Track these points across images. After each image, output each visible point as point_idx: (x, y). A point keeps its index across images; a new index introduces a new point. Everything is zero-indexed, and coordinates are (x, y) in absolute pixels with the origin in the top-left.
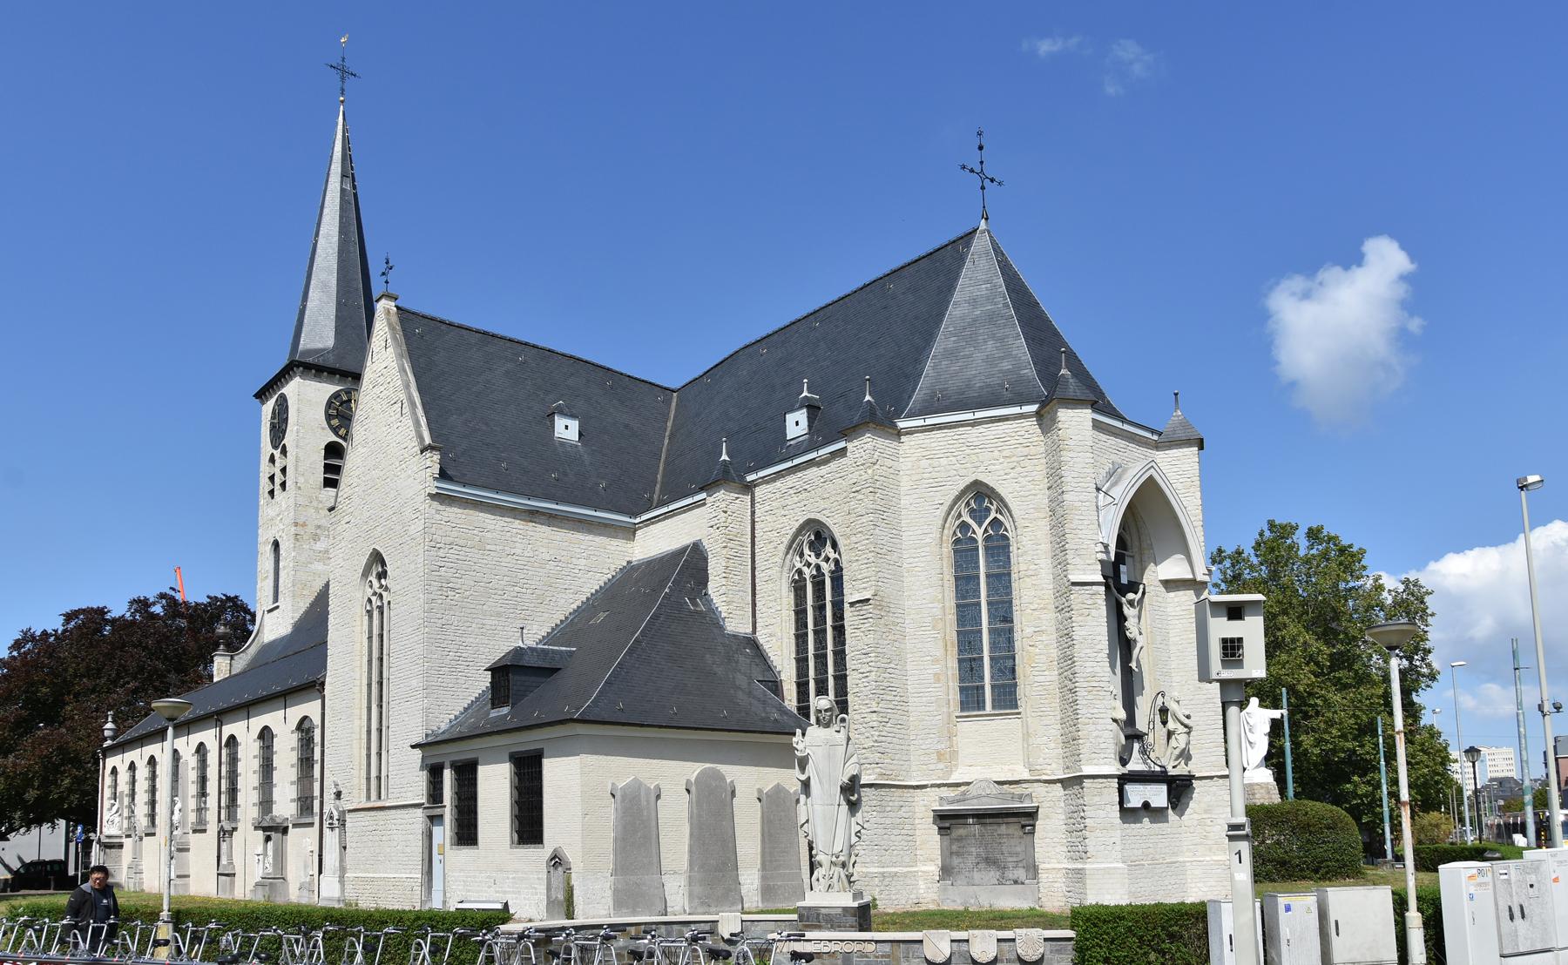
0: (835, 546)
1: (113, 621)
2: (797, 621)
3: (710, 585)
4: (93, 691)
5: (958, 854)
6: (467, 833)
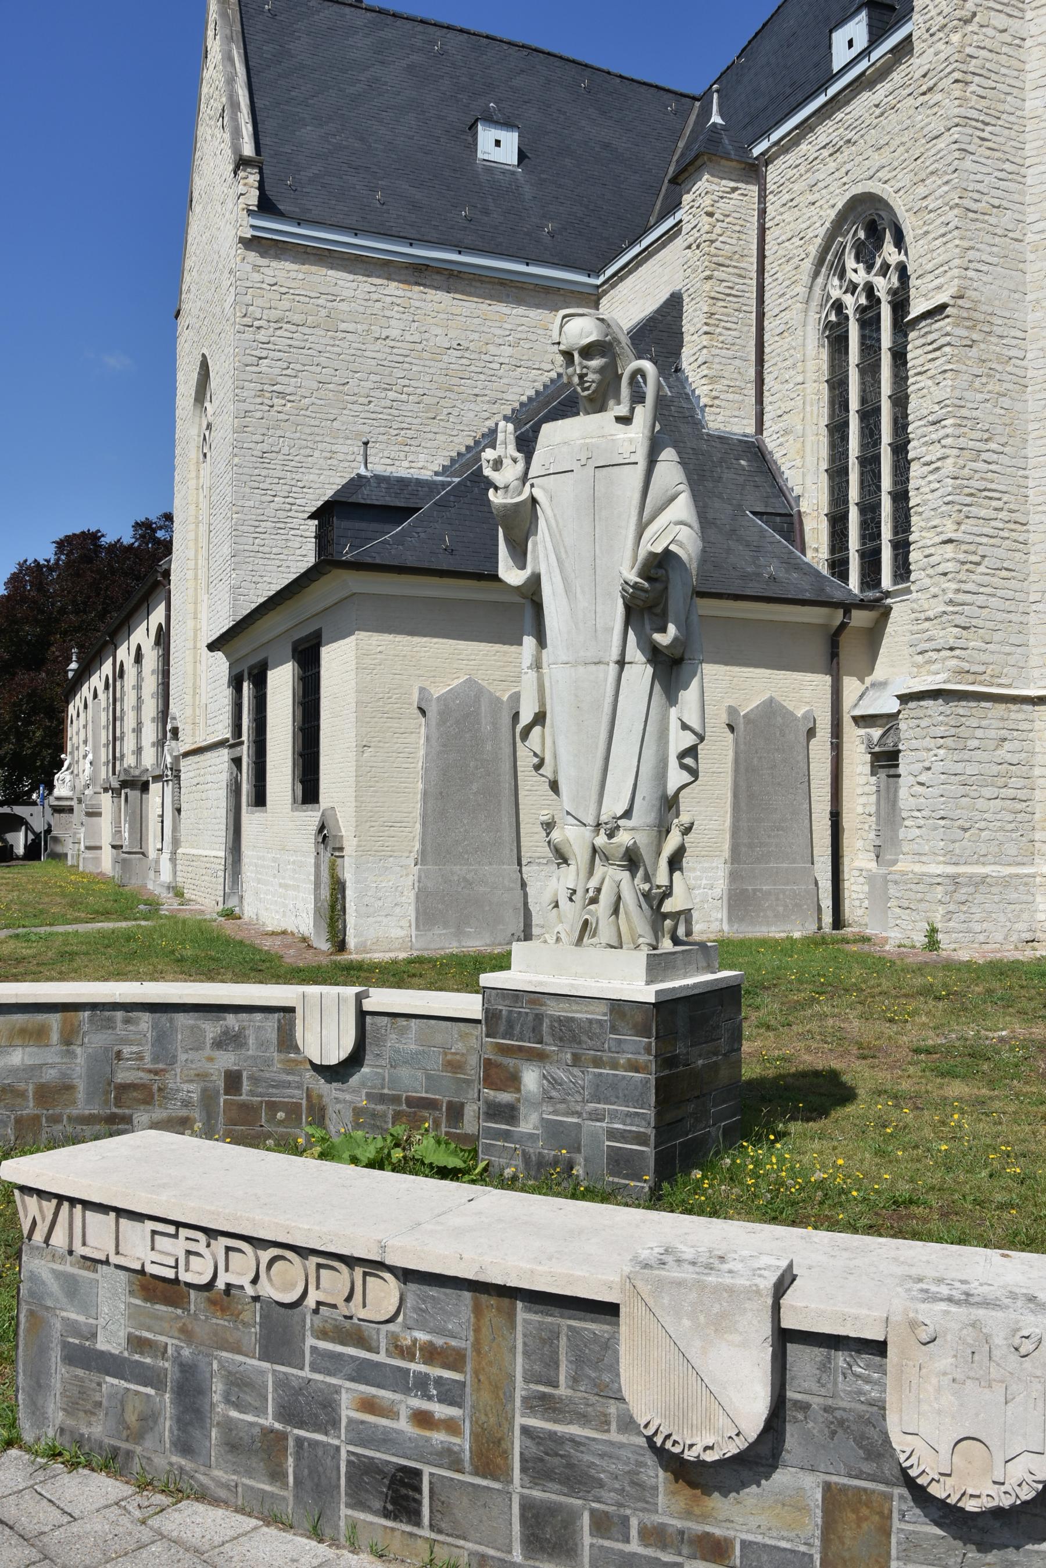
0: (899, 241)
2: (832, 403)
3: (686, 353)
4: (78, 629)
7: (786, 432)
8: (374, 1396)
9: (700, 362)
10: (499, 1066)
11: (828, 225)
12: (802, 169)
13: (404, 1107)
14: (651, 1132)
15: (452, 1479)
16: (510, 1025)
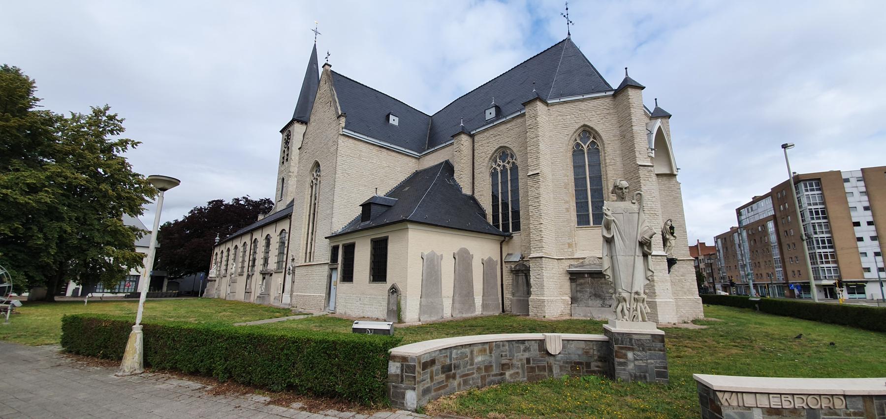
1: (226, 205)
5: (580, 292)
6: (348, 276)
14: (617, 367)
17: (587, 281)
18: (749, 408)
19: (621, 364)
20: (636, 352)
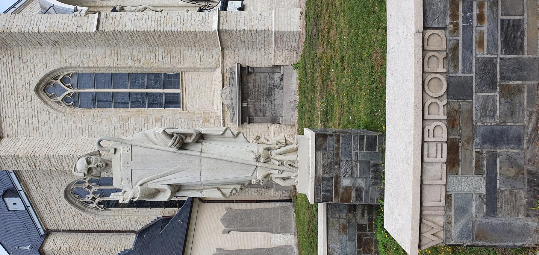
5: (265, 113)
7: (137, 222)
8: (476, 41)
9: (109, 252)
10: (342, 197)
11: (72, 207)
12: (52, 216)
13: (361, 249)
15: (501, 5)
16: (327, 191)
17: (250, 97)
18: (448, 197)
19: (359, 197)
20: (342, 174)
